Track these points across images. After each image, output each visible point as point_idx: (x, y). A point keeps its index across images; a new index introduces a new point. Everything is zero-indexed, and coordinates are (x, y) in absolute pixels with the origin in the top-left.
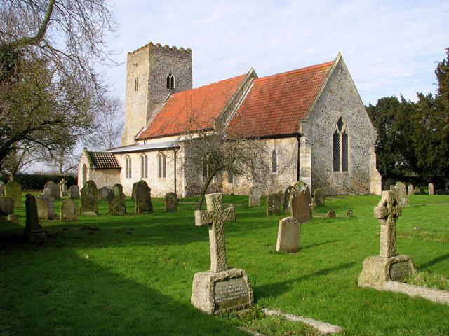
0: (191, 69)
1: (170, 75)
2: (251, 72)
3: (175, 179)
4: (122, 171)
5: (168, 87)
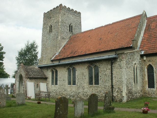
0: (81, 22)
1: (71, 24)
2: (144, 13)
3: (112, 86)
4: (48, 80)
5: (70, 31)
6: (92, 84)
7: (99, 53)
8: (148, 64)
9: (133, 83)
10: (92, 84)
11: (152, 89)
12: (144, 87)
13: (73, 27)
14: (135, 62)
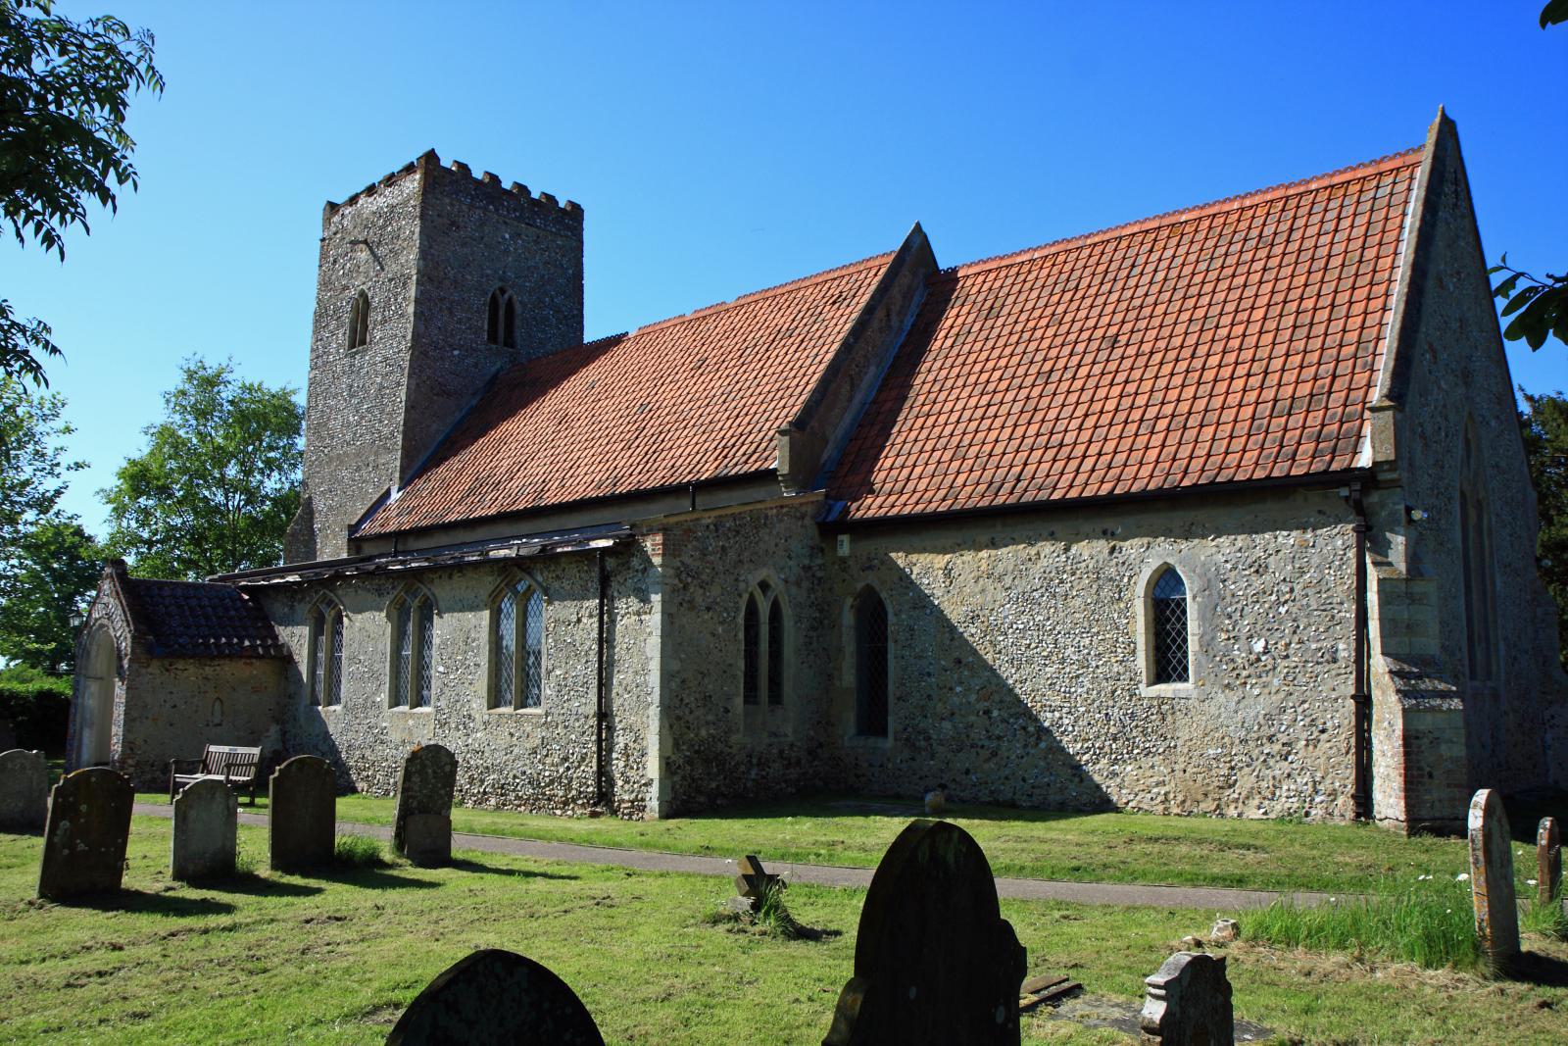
1: (503, 291)
3: (604, 715)
5: (493, 337)
6: (756, 703)
7: (548, 515)
8: (860, 586)
9: (739, 701)
10: (756, 703)
11: (872, 740)
12: (833, 725)
13: (518, 307)
14: (763, 574)
